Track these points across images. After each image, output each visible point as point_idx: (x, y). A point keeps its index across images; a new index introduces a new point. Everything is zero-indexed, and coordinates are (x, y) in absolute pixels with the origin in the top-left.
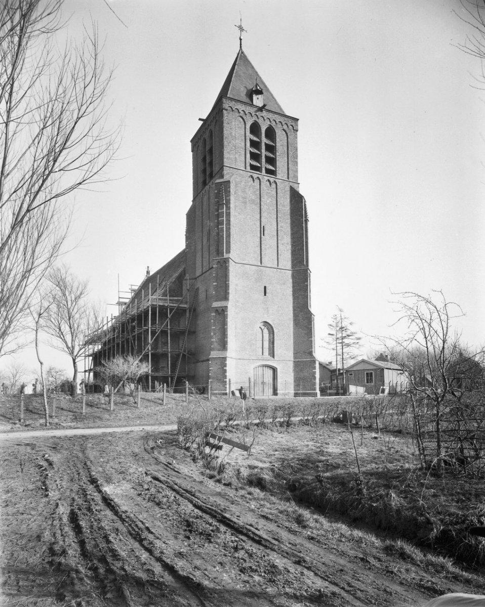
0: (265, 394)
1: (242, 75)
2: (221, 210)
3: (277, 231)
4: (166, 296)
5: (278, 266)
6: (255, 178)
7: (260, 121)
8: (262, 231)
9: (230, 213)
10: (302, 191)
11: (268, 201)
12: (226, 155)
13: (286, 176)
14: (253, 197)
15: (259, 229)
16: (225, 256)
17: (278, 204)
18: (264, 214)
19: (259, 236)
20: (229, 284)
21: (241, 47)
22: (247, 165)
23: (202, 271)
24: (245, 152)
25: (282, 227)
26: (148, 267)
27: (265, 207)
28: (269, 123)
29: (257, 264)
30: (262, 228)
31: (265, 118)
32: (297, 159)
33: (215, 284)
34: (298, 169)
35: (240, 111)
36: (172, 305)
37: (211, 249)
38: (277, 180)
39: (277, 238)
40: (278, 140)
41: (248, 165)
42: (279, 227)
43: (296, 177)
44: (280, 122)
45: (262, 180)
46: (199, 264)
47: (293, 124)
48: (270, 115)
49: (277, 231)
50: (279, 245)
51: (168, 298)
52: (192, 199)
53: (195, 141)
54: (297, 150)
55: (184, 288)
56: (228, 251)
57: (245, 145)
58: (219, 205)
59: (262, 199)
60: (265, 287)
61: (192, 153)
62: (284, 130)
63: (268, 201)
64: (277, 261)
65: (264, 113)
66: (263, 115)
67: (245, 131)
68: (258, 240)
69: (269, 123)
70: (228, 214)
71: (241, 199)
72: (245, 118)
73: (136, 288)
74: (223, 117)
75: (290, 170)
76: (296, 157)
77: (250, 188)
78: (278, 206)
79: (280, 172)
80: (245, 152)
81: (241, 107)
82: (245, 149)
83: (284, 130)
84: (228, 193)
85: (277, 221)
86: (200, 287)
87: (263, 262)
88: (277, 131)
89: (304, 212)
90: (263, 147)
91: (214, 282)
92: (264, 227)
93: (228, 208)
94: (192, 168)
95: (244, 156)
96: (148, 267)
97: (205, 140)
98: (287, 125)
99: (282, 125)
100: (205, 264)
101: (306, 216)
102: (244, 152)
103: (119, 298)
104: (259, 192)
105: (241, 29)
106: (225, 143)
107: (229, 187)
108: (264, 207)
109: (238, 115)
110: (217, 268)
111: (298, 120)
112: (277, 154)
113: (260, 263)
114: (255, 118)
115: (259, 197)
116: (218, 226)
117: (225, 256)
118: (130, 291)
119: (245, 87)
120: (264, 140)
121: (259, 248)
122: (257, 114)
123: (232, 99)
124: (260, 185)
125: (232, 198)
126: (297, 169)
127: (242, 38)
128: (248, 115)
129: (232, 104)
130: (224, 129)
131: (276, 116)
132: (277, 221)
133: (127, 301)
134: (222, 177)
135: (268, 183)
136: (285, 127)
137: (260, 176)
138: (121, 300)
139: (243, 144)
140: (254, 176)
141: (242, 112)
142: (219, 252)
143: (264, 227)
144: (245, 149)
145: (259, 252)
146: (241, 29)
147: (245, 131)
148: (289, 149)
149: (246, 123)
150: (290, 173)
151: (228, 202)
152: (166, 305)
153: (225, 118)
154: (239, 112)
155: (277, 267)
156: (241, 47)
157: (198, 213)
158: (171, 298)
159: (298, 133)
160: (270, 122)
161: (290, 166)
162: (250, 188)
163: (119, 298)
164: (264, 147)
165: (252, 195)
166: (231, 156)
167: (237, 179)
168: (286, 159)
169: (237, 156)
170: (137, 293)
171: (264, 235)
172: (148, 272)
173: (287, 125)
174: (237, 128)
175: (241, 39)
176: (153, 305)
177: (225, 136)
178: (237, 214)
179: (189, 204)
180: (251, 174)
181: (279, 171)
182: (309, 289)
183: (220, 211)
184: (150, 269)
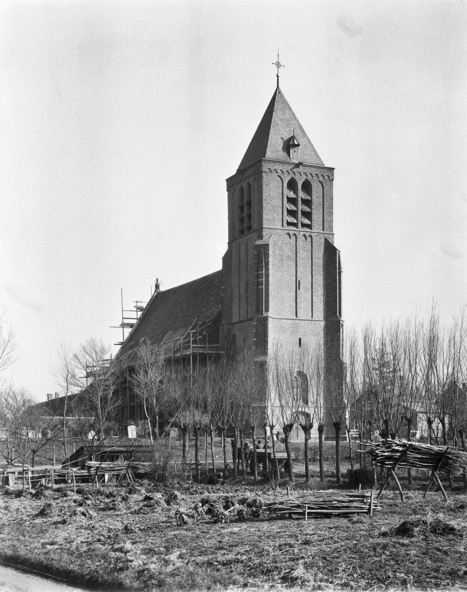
0: (299, 438)
1: (279, 122)
2: (261, 271)
3: (312, 283)
4: (206, 344)
5: (312, 317)
6: (291, 235)
7: (297, 177)
8: (298, 285)
9: (268, 274)
10: (337, 244)
11: (303, 255)
12: (265, 217)
13: (321, 228)
14: (290, 254)
15: (295, 284)
16: (265, 314)
17: (314, 257)
18: (300, 269)
19: (295, 290)
20: (267, 340)
21: (278, 85)
22: (284, 223)
23: (239, 319)
24: (283, 210)
25: (316, 279)
26: (157, 280)
27: (301, 261)
28: (305, 177)
29: (292, 318)
30: (298, 283)
31: (302, 173)
32: (332, 209)
33: (255, 339)
34: (333, 219)
35: (278, 171)
36: (210, 352)
37: (249, 300)
38: (312, 234)
39: (312, 291)
40: (314, 192)
41: (285, 222)
42: (313, 280)
43: (331, 228)
44: (316, 174)
45: (298, 236)
46: (235, 311)
47: (329, 174)
48: (307, 170)
49: (312, 283)
50: (314, 297)
51: (207, 345)
52: (227, 241)
53: (231, 183)
54: (332, 199)
55: (220, 333)
56: (267, 310)
57: (283, 203)
58: (259, 269)
59: (298, 255)
60: (300, 339)
61: (227, 192)
62: (320, 181)
63: (303, 255)
64: (311, 313)
65: (301, 169)
66: (299, 171)
67: (283, 190)
68: (294, 294)
69: (305, 177)
70: (267, 276)
71: (278, 257)
72: (282, 176)
73: (144, 305)
74: (262, 179)
75: (325, 222)
76: (331, 207)
77: (286, 245)
78: (313, 260)
79: (315, 225)
80: (283, 210)
81: (279, 167)
82: (283, 208)
83: (320, 181)
84: (267, 255)
85: (312, 274)
86: (237, 334)
87: (298, 315)
88: (313, 184)
89: (338, 263)
90: (300, 202)
91: (254, 338)
92: (299, 281)
93: (267, 269)
94: (227, 215)
95: (281, 214)
96: (157, 280)
97: (242, 189)
98: (323, 176)
99: (318, 177)
100: (242, 313)
101: (340, 268)
102: (281, 210)
103: (123, 318)
104: (294, 248)
105: (278, 65)
106: (264, 205)
107: (268, 250)
108: (300, 262)
109: (276, 174)
110: (257, 325)
111: (334, 169)
112: (313, 207)
113: (295, 316)
114: (292, 175)
115: (295, 253)
116: (258, 286)
117: (265, 314)
118: (135, 309)
119: (282, 138)
120: (302, 195)
121: (295, 302)
122: (294, 170)
123: (270, 161)
124: (296, 240)
125: (271, 259)
126: (332, 219)
127: (279, 75)
128: (286, 173)
129: (271, 166)
130: (264, 192)
131: (312, 169)
132: (312, 274)
133: (135, 321)
134: (261, 237)
135: (304, 238)
136: (321, 178)
137: (296, 232)
138: (126, 321)
139: (281, 202)
140: (290, 233)
141: (280, 172)
142: (259, 311)
143: (299, 281)
144: (283, 208)
145: (294, 306)
146: (278, 65)
147: (283, 190)
148: (325, 200)
149: (284, 181)
150: (325, 224)
151: (267, 264)
152: (205, 352)
153: (264, 180)
154: (277, 172)
155: (311, 319)
156: (278, 85)
157: (234, 257)
158: (210, 346)
159: (334, 182)
160: (306, 176)
161: (325, 217)
162: (286, 245)
163: (123, 318)
164: (301, 202)
165: (288, 251)
166: (270, 217)
167: (275, 239)
168: (321, 210)
169: (275, 215)
170: (146, 313)
171: (299, 289)
172: (157, 286)
173: (323, 176)
174: (275, 188)
175: (278, 77)
176: (193, 353)
177: (264, 197)
178: (274, 272)
179: (225, 248)
180: (288, 231)
181: (314, 224)
182: (341, 337)
183: (259, 272)
184: (159, 282)
